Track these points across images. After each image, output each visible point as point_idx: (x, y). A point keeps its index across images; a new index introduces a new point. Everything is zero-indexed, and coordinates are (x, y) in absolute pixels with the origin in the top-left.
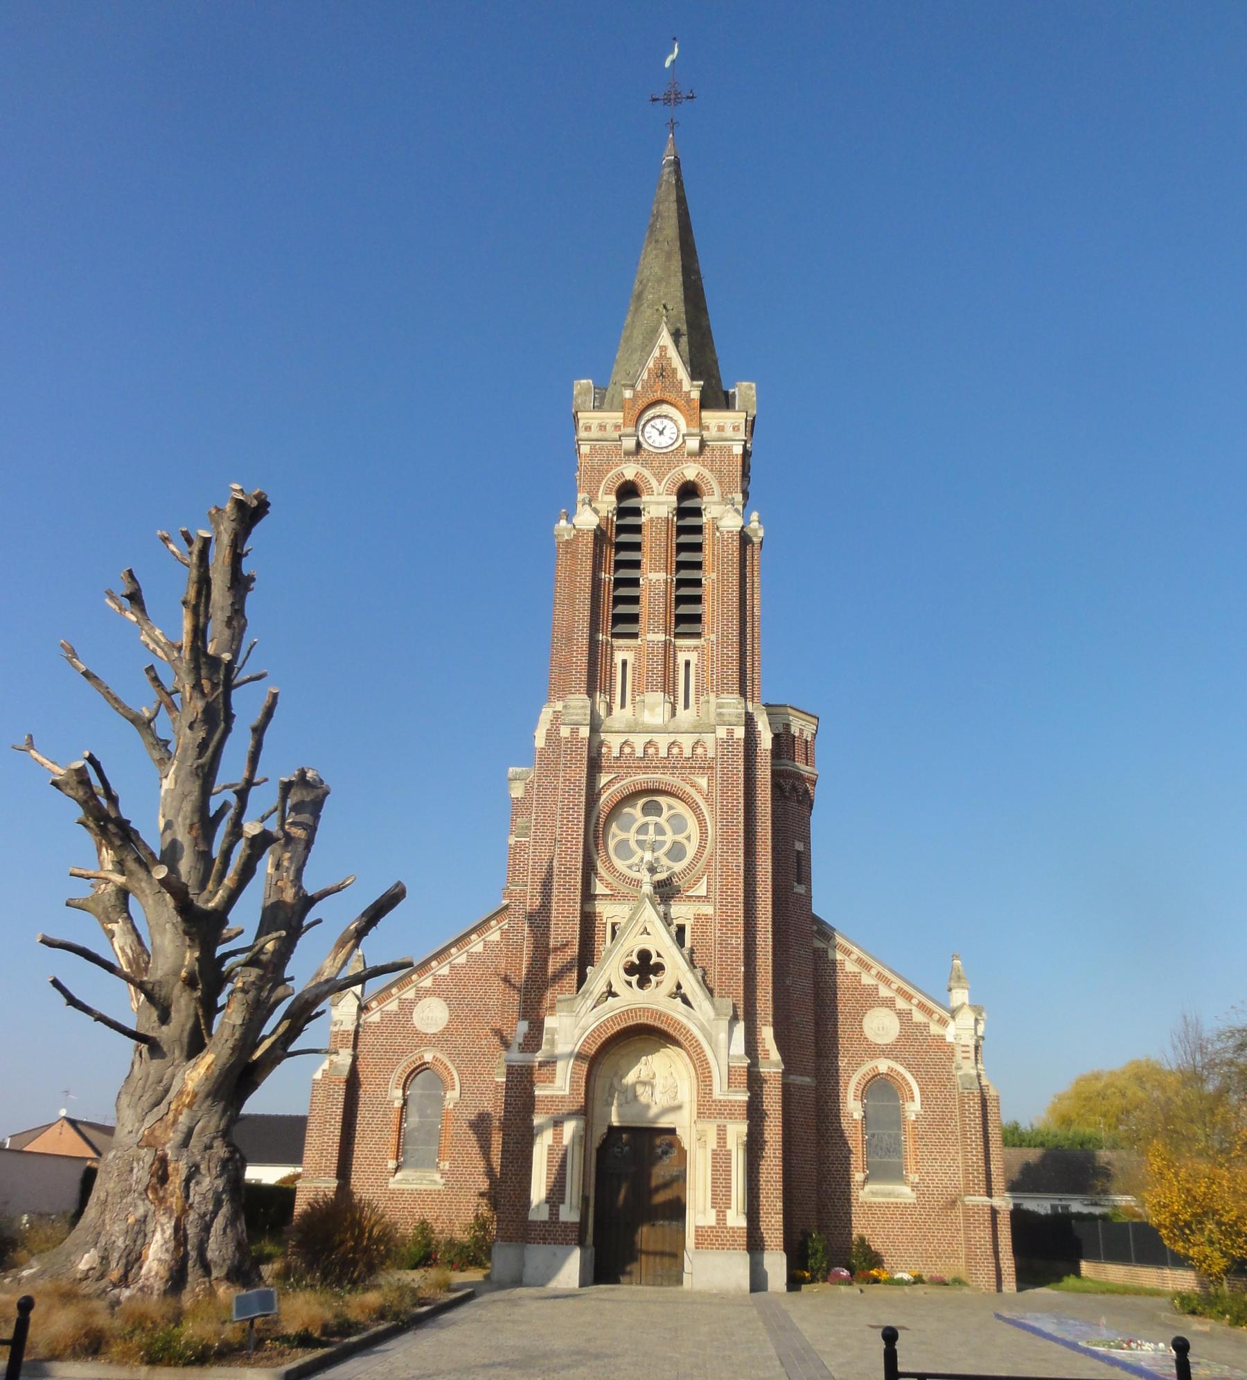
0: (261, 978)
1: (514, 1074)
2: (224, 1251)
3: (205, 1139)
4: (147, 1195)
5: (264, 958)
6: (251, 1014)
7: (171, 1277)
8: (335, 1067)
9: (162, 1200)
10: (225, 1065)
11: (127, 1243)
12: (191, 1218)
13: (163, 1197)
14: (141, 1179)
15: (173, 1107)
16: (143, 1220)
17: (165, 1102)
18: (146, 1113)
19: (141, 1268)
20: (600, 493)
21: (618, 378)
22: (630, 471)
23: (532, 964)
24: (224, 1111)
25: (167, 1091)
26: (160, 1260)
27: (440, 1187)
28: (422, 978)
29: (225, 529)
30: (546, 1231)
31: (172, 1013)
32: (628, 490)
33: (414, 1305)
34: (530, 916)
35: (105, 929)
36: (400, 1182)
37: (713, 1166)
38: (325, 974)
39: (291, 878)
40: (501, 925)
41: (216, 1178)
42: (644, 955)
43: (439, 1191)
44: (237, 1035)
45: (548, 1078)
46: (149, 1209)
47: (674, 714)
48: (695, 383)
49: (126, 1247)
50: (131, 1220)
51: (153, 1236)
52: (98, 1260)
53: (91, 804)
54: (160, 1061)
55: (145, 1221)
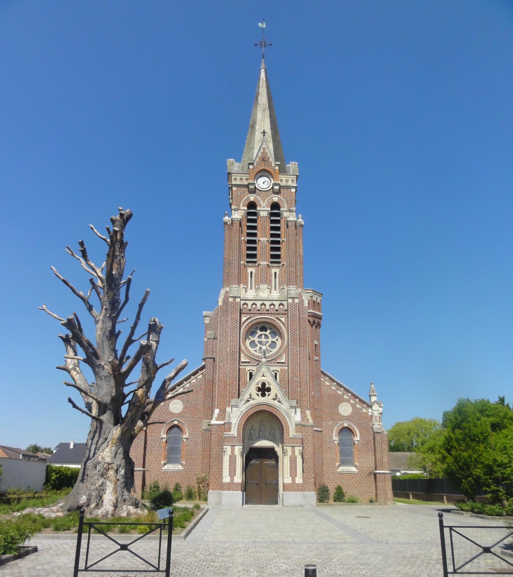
11: (97, 493)
14: (100, 470)
21: (245, 159)
22: (252, 198)
30: (229, 486)
32: (252, 205)
37: (290, 462)
42: (264, 384)
45: (228, 430)
47: (271, 292)
48: (277, 163)
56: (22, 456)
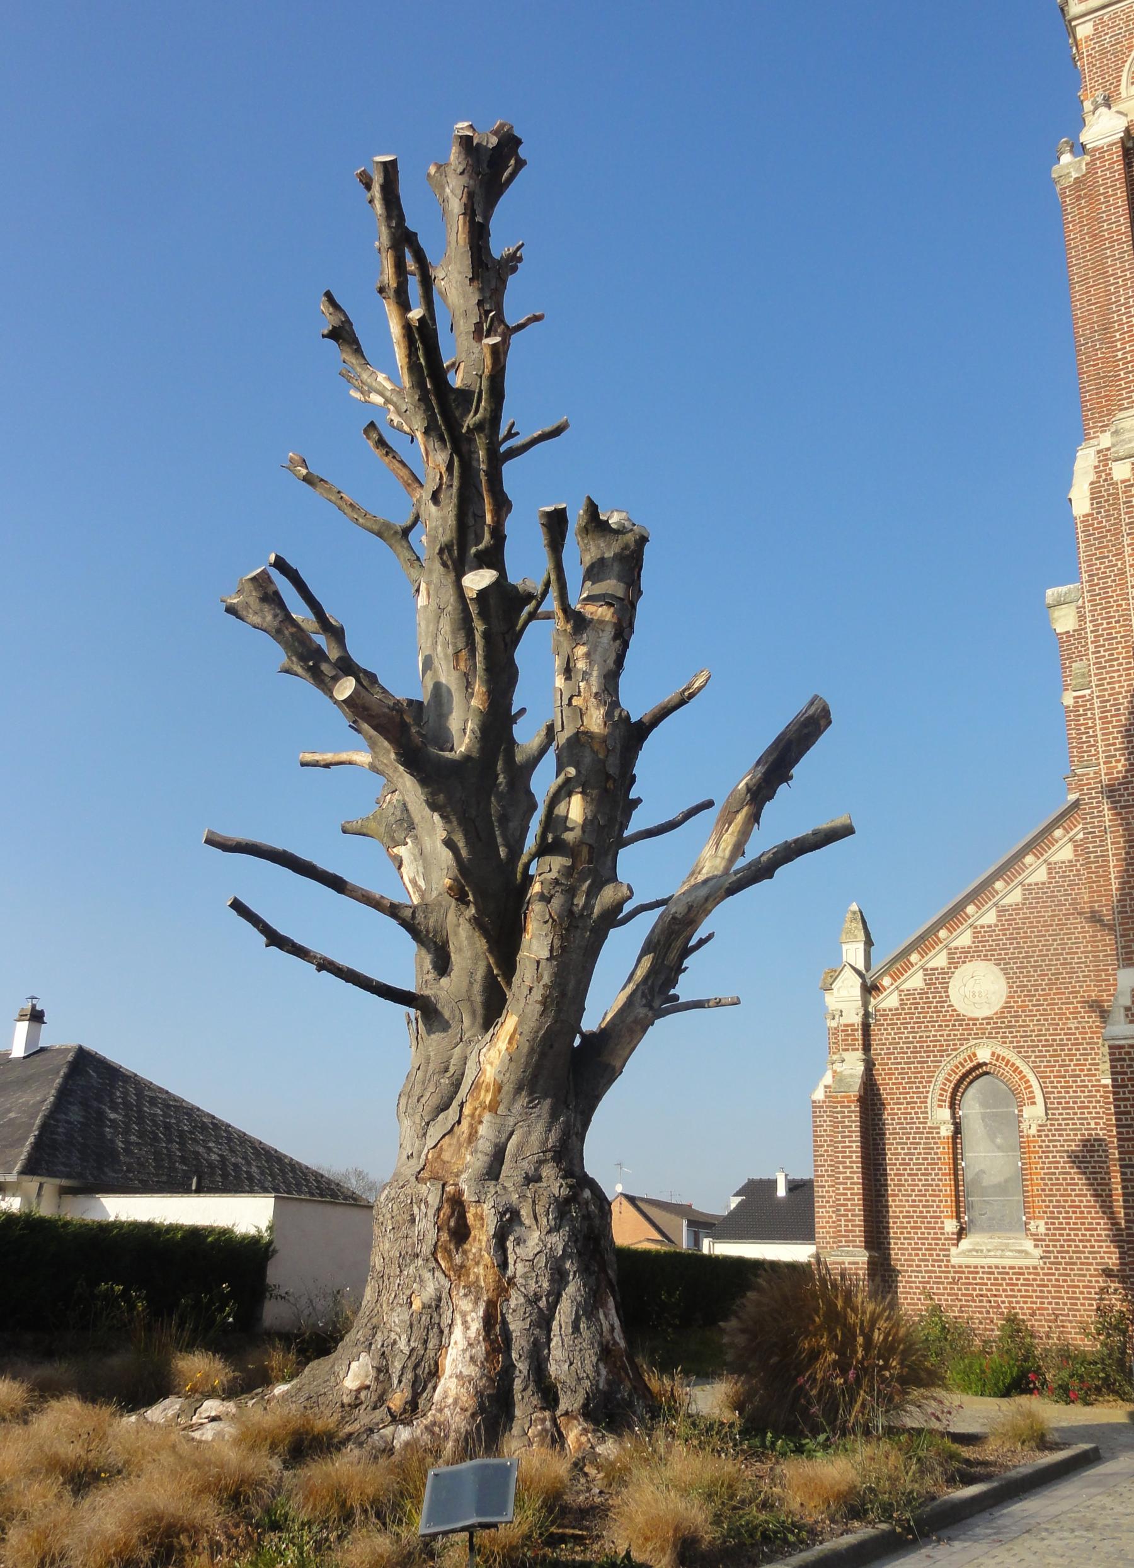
0: (568, 872)
1: (1124, 1060)
2: (577, 1363)
3: (525, 1165)
4: (436, 1260)
5: (569, 837)
6: (562, 938)
7: (481, 1409)
8: (841, 1080)
9: (461, 1270)
10: (537, 1032)
11: (413, 1344)
12: (513, 1303)
13: (462, 1266)
15: (467, 1111)
16: (435, 1306)
17: (455, 1104)
18: (428, 1124)
19: (434, 1388)
20: (1123, 88)
23: (1127, 871)
24: (554, 1116)
25: (457, 1085)
26: (460, 1376)
27: (1035, 1262)
28: (955, 934)
29: (452, 191)
31: (452, 954)
33: (951, 1481)
34: (1111, 791)
35: (390, 855)
36: (967, 1253)
38: (704, 871)
39: (594, 690)
40: (1072, 833)
41: (549, 1232)
43: (1035, 1268)
44: (546, 979)
46: (443, 1286)
49: (412, 1350)
50: (417, 1305)
51: (450, 1333)
52: (372, 1373)
53: (286, 632)
54: (442, 1035)
55: (438, 1307)
56: (688, 1226)
